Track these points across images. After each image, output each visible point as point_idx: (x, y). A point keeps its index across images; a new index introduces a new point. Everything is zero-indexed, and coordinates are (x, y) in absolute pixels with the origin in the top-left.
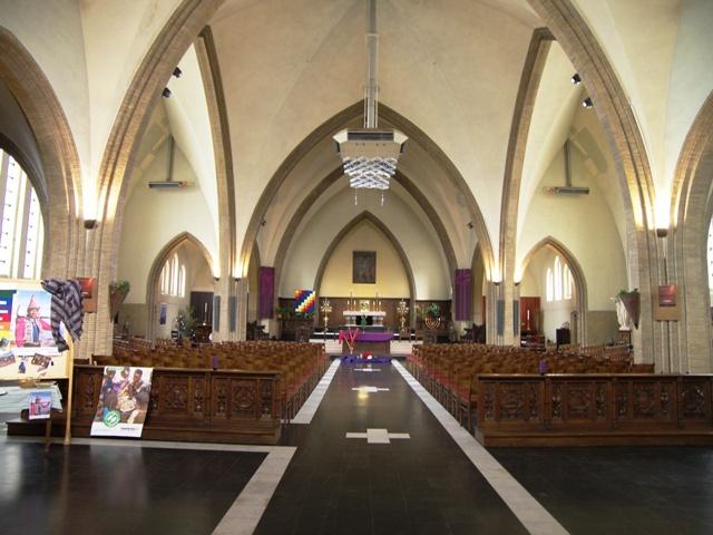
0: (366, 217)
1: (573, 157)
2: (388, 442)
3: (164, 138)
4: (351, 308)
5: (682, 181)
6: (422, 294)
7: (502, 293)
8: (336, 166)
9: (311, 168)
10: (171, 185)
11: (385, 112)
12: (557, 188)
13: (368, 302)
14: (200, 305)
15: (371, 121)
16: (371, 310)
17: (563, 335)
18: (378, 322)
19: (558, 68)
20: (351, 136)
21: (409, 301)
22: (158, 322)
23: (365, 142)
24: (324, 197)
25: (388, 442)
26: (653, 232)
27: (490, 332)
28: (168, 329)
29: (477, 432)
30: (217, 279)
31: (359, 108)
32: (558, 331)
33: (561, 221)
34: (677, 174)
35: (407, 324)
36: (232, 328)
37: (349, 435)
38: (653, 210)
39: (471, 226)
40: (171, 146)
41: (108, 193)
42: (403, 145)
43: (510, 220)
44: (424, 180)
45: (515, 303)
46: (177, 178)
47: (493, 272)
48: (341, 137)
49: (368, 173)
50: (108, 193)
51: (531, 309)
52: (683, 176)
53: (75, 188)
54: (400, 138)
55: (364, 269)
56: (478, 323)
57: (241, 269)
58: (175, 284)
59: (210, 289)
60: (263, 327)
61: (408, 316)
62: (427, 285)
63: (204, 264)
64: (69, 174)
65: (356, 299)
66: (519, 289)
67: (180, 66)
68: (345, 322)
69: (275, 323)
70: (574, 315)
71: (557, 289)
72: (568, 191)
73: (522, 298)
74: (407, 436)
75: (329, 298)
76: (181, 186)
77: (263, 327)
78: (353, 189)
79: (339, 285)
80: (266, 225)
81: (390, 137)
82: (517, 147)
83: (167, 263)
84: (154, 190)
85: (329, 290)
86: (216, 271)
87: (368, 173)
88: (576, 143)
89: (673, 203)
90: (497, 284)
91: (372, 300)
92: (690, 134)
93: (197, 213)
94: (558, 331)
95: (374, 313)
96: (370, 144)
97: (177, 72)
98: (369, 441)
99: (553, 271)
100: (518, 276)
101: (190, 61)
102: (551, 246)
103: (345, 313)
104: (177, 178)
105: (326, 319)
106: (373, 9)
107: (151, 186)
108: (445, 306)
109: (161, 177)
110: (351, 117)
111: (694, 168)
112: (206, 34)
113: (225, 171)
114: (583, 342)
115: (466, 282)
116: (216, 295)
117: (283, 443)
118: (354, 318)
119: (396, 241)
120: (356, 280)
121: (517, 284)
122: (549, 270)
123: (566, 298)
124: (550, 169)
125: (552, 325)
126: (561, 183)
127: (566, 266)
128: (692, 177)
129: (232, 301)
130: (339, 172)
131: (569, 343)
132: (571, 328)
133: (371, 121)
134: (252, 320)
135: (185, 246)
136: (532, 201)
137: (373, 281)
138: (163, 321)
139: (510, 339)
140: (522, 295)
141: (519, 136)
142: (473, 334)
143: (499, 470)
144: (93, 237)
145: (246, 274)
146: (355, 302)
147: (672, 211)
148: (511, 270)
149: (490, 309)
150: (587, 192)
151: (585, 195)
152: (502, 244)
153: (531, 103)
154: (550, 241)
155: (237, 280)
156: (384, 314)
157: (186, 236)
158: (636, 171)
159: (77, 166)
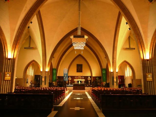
0: (80, 55)
1: (131, 40)
2: (79, 110)
3: (27, 37)
4: (76, 79)
5: (152, 48)
6: (94, 75)
7: (113, 75)
8: (71, 44)
9: (64, 44)
10: (30, 48)
11: (83, 29)
12: (127, 48)
13: (80, 77)
14: (37, 79)
15: (79, 33)
16: (81, 79)
17: (130, 85)
18: (83, 82)
19: (124, 20)
20: (74, 37)
21: (91, 77)
22: (26, 83)
23: (78, 38)
24: (67, 53)
25: (79, 110)
26: (145, 60)
27: (111, 84)
28: (28, 85)
29: (101, 109)
30: (42, 72)
31: (76, 29)
32: (128, 84)
33: (129, 57)
34: (151, 46)
35: (90, 82)
36: (45, 84)
37: (71, 108)
38: (145, 55)
39: (105, 58)
40: (30, 38)
41: (14, 53)
42: (87, 39)
43: (115, 56)
44: (94, 46)
45: (117, 77)
46: (31, 46)
47: (111, 70)
48: (72, 37)
49: (79, 45)
50: (14, 53)
51: (122, 78)
52: (152, 46)
53: (6, 50)
54: (86, 37)
55: (80, 69)
56: (108, 82)
57: (47, 69)
58: (31, 72)
59: (40, 74)
60: (54, 84)
61: (90, 81)
62: (95, 72)
63: (39, 68)
64: (5, 47)
65: (77, 76)
66: (118, 74)
67: (32, 21)
68: (75, 82)
69: (56, 83)
70: (132, 80)
71: (128, 73)
72: (130, 49)
73: (118, 76)
74: (84, 109)
75: (70, 76)
76: (33, 48)
77: (54, 84)
78: (75, 49)
79: (73, 73)
80: (54, 58)
81: (84, 37)
82: (116, 38)
83: (29, 67)
84: (25, 49)
85: (71, 74)
86: (41, 70)
87: (79, 45)
88: (132, 37)
89: (150, 53)
90: (112, 72)
91: (81, 76)
92: (153, 37)
93: (37, 55)
94: (128, 84)
95: (82, 80)
96: (79, 39)
97: (31, 23)
98: (75, 110)
99: (127, 69)
100: (117, 70)
101: (35, 20)
102: (125, 63)
103: (74, 80)
104: (31, 46)
105: (89, 81)
106: (79, 2)
107: (25, 48)
108: (100, 78)
109: (27, 46)
110: (73, 32)
111: (154, 44)
112: (39, 12)
113: (44, 45)
114: (135, 87)
115: (105, 71)
116: (41, 76)
117: (55, 110)
118: (77, 81)
119: (87, 60)
120: (77, 71)
121: (117, 72)
122: (126, 69)
123: (130, 76)
124: (125, 43)
125: (128, 82)
126: (128, 47)
127: (130, 68)
128: (154, 47)
129: (45, 77)
130: (71, 45)
131: (132, 87)
132: (132, 84)
133: (79, 33)
134: (51, 82)
135: (34, 63)
136: (121, 51)
137: (82, 72)
138: (27, 83)
139: (115, 87)
140: (119, 75)
141: (116, 35)
142: (106, 85)
143: (103, 116)
144: (10, 62)
145: (49, 70)
146: (77, 77)
147: (150, 55)
148: (115, 69)
149: (110, 79)
150: (135, 49)
151: (134, 50)
152: (113, 62)
153: (119, 27)
154: (125, 62)
155: (47, 72)
156: (84, 80)
157: (34, 61)
158: (141, 45)
159: (6, 45)
